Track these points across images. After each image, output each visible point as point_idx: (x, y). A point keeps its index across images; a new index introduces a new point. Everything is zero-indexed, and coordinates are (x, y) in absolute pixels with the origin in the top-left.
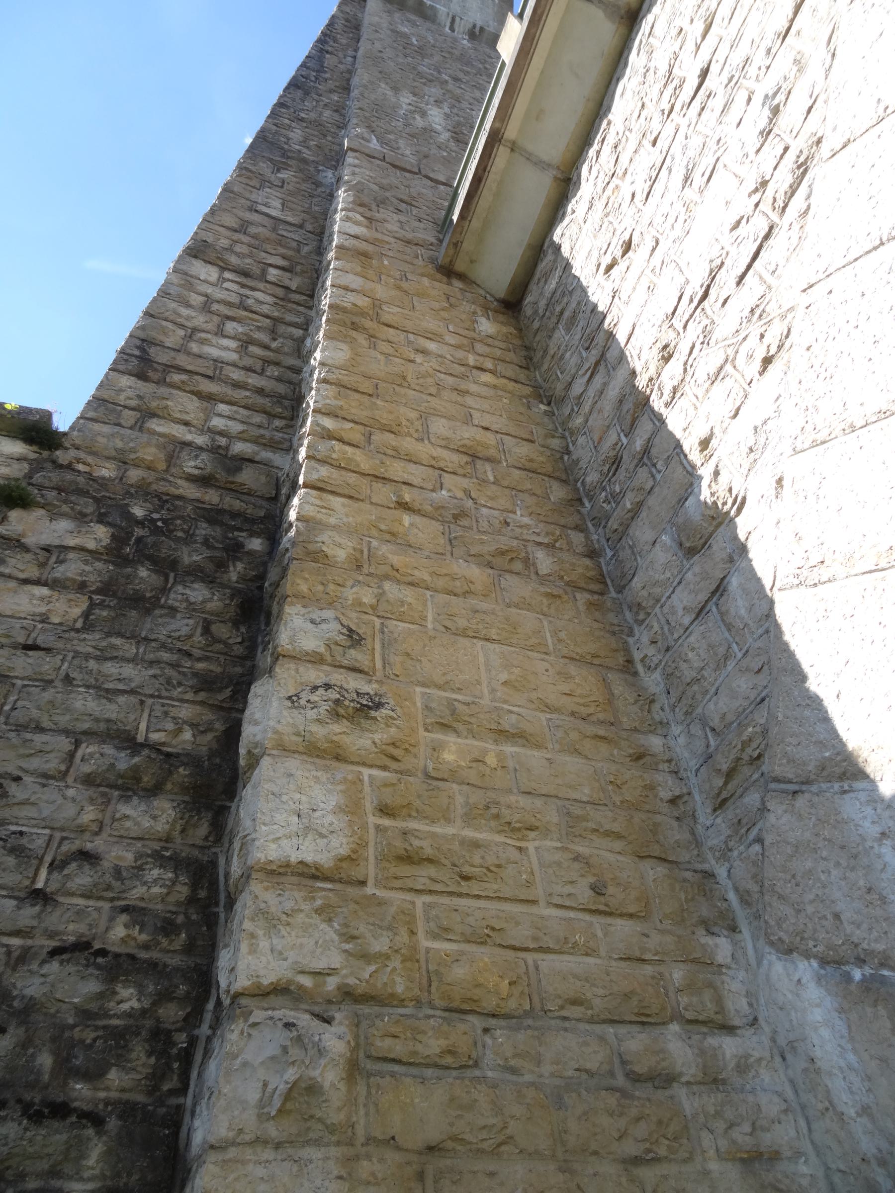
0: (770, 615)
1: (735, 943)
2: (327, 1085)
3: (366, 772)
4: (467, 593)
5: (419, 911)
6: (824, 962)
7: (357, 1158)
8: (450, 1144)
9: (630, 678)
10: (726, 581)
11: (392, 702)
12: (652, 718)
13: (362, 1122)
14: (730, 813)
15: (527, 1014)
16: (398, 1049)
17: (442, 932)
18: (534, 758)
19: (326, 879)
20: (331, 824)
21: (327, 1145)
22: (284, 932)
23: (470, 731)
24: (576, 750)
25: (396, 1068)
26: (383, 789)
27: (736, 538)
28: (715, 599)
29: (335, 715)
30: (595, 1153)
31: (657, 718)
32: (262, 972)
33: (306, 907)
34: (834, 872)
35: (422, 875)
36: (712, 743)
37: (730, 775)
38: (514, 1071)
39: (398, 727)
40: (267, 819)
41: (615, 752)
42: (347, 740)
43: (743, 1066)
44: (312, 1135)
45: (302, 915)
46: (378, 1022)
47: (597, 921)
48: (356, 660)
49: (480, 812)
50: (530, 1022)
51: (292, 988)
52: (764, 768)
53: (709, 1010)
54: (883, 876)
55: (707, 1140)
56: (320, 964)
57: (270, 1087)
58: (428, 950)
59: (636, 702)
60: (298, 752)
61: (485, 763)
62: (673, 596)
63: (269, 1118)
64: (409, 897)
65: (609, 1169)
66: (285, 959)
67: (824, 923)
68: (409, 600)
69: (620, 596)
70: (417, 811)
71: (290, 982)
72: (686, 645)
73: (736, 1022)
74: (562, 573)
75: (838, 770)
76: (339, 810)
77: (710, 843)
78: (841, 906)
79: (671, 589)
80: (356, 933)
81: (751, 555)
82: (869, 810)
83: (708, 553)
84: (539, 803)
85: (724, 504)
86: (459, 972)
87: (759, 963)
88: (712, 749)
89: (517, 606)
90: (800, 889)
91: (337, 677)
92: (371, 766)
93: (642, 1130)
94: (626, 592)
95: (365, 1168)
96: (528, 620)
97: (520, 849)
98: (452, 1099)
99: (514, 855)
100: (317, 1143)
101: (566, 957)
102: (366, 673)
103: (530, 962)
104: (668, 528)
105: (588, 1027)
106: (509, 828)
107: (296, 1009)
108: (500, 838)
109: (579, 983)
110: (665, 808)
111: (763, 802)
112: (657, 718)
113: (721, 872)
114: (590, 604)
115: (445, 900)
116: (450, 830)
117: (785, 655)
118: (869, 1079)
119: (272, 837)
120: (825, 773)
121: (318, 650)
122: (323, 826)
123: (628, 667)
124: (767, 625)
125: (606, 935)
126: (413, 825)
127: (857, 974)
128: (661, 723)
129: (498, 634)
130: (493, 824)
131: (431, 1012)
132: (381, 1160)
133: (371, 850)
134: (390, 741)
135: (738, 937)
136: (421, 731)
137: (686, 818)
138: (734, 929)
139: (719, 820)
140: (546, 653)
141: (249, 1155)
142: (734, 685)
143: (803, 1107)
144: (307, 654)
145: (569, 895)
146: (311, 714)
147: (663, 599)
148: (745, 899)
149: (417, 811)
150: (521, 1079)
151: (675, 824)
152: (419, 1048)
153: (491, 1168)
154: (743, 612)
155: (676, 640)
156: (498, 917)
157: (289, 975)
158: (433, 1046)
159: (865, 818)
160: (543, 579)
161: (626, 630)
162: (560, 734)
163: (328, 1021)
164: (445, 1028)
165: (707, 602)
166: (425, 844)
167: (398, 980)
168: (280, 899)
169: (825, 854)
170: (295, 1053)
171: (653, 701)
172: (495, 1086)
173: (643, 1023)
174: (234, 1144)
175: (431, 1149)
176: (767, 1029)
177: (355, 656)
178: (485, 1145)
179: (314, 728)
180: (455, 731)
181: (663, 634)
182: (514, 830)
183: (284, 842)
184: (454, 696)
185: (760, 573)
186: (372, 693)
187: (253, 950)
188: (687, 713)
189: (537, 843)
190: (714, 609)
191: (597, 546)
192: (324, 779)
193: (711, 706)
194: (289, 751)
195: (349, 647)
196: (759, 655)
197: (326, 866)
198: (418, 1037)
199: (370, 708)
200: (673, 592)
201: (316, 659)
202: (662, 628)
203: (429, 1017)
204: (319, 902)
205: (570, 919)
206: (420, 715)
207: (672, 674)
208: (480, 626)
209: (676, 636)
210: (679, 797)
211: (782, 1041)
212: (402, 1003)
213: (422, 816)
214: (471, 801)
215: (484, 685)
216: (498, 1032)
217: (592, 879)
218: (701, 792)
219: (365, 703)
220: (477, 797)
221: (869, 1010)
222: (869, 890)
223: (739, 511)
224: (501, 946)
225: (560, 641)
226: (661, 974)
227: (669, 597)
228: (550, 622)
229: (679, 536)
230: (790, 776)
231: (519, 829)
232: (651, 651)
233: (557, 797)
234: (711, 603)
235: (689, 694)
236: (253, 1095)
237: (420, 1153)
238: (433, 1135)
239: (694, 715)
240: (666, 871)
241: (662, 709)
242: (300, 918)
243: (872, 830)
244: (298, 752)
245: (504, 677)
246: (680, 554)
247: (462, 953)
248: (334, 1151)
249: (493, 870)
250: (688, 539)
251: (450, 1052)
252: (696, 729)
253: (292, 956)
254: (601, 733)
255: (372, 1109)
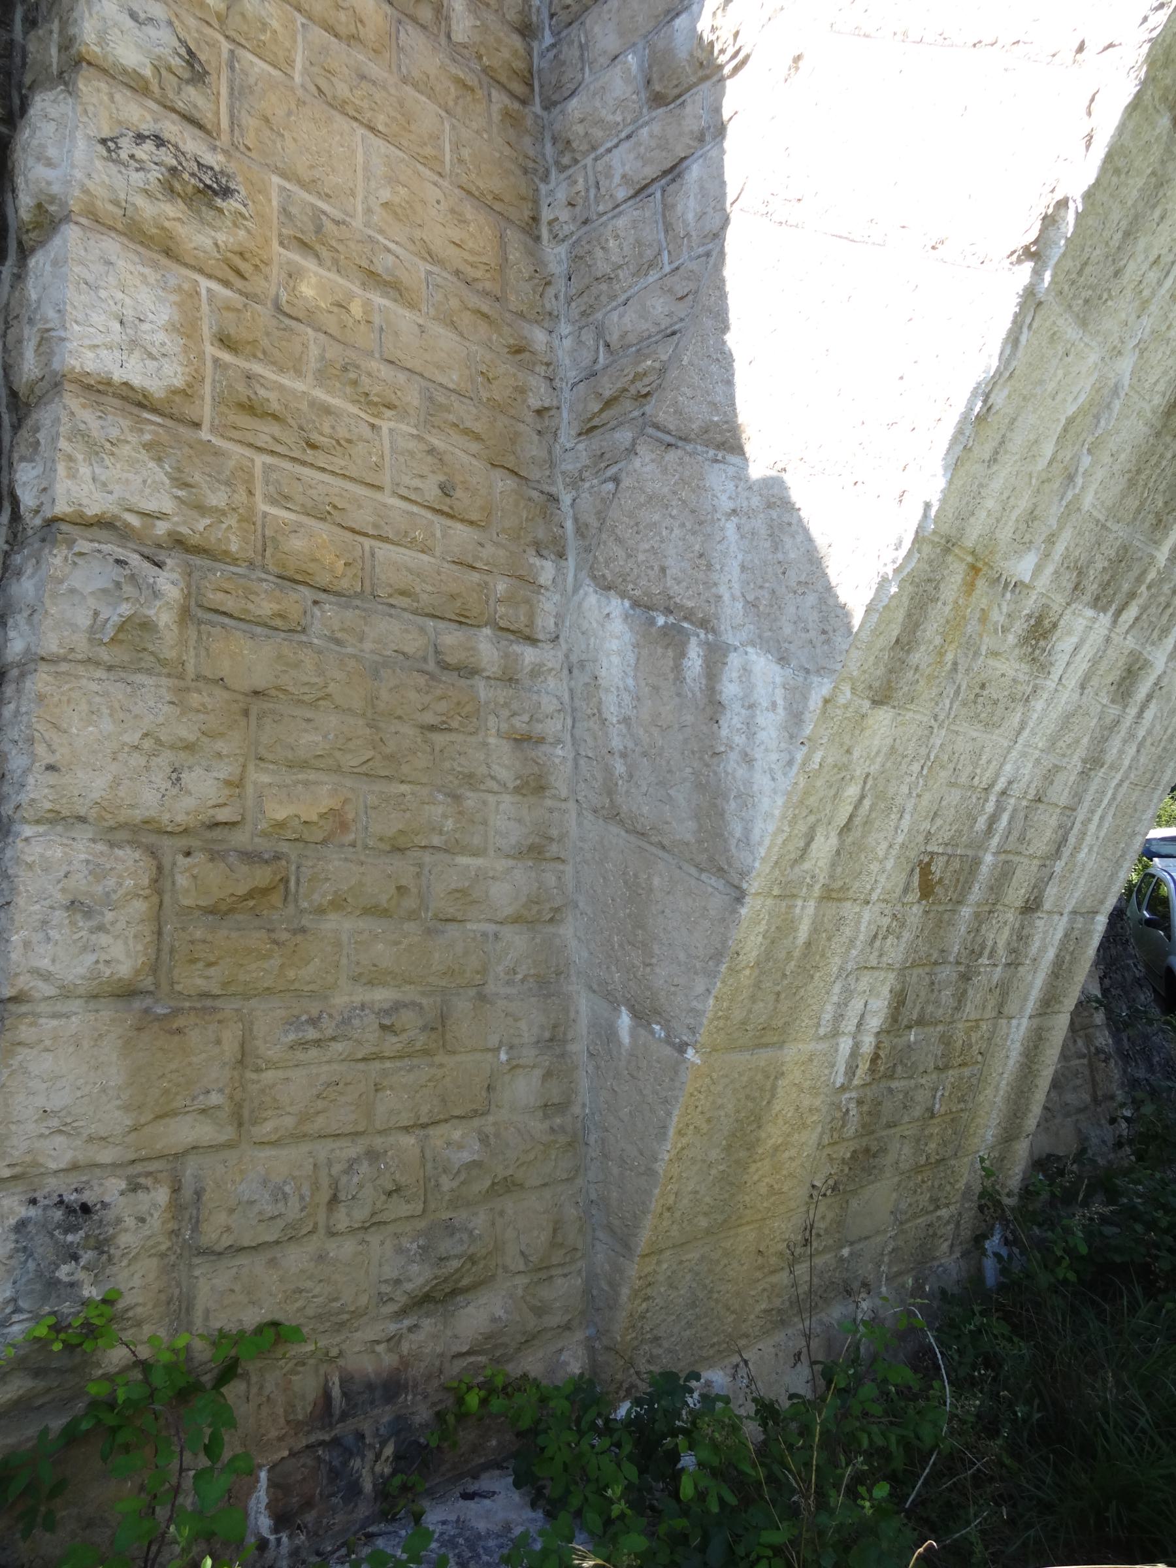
0: (717, 236)
1: (559, 569)
2: (161, 624)
3: (205, 283)
4: (353, 39)
5: (258, 471)
6: (636, 604)
7: (188, 689)
8: (273, 692)
9: (531, 243)
10: (685, 164)
11: (243, 192)
12: (543, 306)
13: (192, 661)
14: (597, 442)
15: (357, 595)
16: (230, 604)
17: (281, 499)
18: (405, 318)
19: (155, 411)
20: (163, 344)
21: (159, 675)
22: (107, 462)
23: (336, 262)
24: (452, 322)
25: (227, 620)
26: (225, 314)
27: (717, 110)
28: (663, 181)
29: (170, 191)
30: (400, 718)
31: (548, 307)
32: (85, 501)
33: (133, 438)
34: (677, 531)
35: (265, 432)
36: (601, 359)
37: (609, 403)
38: (338, 642)
39: (248, 231)
40: (80, 317)
41: (494, 337)
42: (181, 231)
43: (536, 672)
44: (143, 665)
45: (128, 447)
46: (210, 575)
47: (438, 521)
48: (195, 106)
49: (335, 372)
50: (358, 602)
51: (118, 524)
52: (648, 409)
53: (521, 622)
54: (719, 547)
55: (492, 721)
56: (151, 506)
57: (103, 617)
58: (265, 515)
59: (531, 278)
60: (115, 229)
61: (348, 311)
62: (615, 151)
63: (101, 643)
64: (248, 452)
65: (409, 731)
66: (111, 493)
67: (649, 572)
68: (275, 24)
69: (545, 114)
70: (264, 353)
71: (115, 517)
72: (610, 227)
73: (541, 636)
74: (483, 51)
75: (719, 438)
76: (173, 328)
77: (564, 467)
78: (670, 562)
79: (615, 141)
80: (190, 480)
81: (727, 144)
82: (731, 486)
83: (677, 111)
84: (402, 377)
85: (722, 51)
86: (297, 544)
87: (576, 590)
88: (598, 367)
89: (415, 86)
90: (639, 537)
91: (171, 128)
92: (210, 276)
93: (442, 706)
94: (556, 111)
95: (195, 699)
96: (428, 114)
97: (373, 426)
98: (280, 657)
99: (366, 432)
100: (149, 672)
101: (402, 550)
102: (208, 133)
103: (367, 548)
104: (640, 46)
105: (411, 617)
106: (365, 400)
107: (125, 547)
108: (353, 409)
109: (410, 577)
110: (530, 417)
111: (634, 444)
112: (548, 307)
113: (566, 499)
114: (507, 114)
115: (287, 465)
116: (299, 386)
117: (717, 293)
118: (638, 699)
119: (87, 342)
120: (705, 437)
121: (142, 72)
122: (153, 344)
123: (531, 227)
124: (710, 246)
125: (443, 537)
126: (257, 368)
127: (661, 621)
128: (550, 314)
129: (386, 125)
130: (348, 390)
131: (264, 576)
132: (210, 695)
133: (207, 389)
134: (236, 248)
135: (563, 563)
136: (275, 244)
137: (546, 434)
138: (561, 555)
139: (581, 446)
140: (440, 174)
141: (81, 671)
142: (648, 303)
143: (574, 710)
144: (125, 71)
145: (416, 489)
146: (137, 178)
147: (602, 150)
148: (581, 530)
149: (264, 353)
150: (343, 650)
151: (536, 437)
152: (251, 606)
153: (309, 715)
154: (690, 216)
155: (601, 215)
156: (341, 496)
157: (115, 510)
158: (265, 607)
159: (724, 491)
160: (456, 50)
161: (541, 170)
162: (439, 297)
163: (159, 565)
164: (277, 593)
165: (653, 180)
166: (272, 396)
167: (233, 538)
168: (101, 422)
169: (674, 512)
170: (128, 589)
171: (548, 283)
172: (320, 652)
173: (461, 623)
174: (65, 659)
175: (256, 693)
176: (564, 646)
177: (192, 97)
178: (306, 698)
179: (140, 201)
180: (317, 256)
181: (587, 198)
182: (370, 403)
183: (104, 353)
184: (321, 204)
185: (728, 176)
186: (217, 168)
187: (73, 475)
188: (583, 314)
189: (392, 424)
190: (658, 195)
191: (534, 18)
192: (152, 280)
193: (615, 316)
194: (103, 224)
195: (188, 82)
196: (689, 279)
197: (157, 396)
198: (252, 597)
199: (215, 193)
200: (616, 146)
201: (138, 86)
202: (587, 190)
203: (262, 580)
204: (147, 437)
205: (413, 514)
206: (275, 221)
207: (581, 258)
208: (365, 104)
209: (601, 208)
210: (547, 409)
211: (574, 658)
212: (235, 561)
213: (267, 358)
214: (328, 356)
215: (359, 198)
216: (327, 606)
217: (442, 478)
218: (571, 410)
219: (209, 182)
220: (333, 351)
221: (660, 650)
222: (701, 556)
223: (736, 70)
224: (340, 525)
225: (461, 161)
226: (486, 583)
227: (609, 151)
228: (453, 127)
229: (650, 67)
230: (671, 427)
231: (376, 404)
232: (564, 215)
233: (422, 375)
234: (656, 185)
235: (594, 290)
236: (83, 620)
237: (246, 695)
238: (260, 684)
239: (591, 319)
240: (514, 486)
241: (556, 297)
242: (126, 450)
243: (726, 504)
244: (115, 229)
245: (385, 194)
246: (643, 96)
247: (301, 525)
248: (164, 681)
249: (343, 444)
250: (661, 80)
251: (280, 616)
252: (588, 337)
253: (118, 490)
254: (485, 309)
255: (203, 653)
